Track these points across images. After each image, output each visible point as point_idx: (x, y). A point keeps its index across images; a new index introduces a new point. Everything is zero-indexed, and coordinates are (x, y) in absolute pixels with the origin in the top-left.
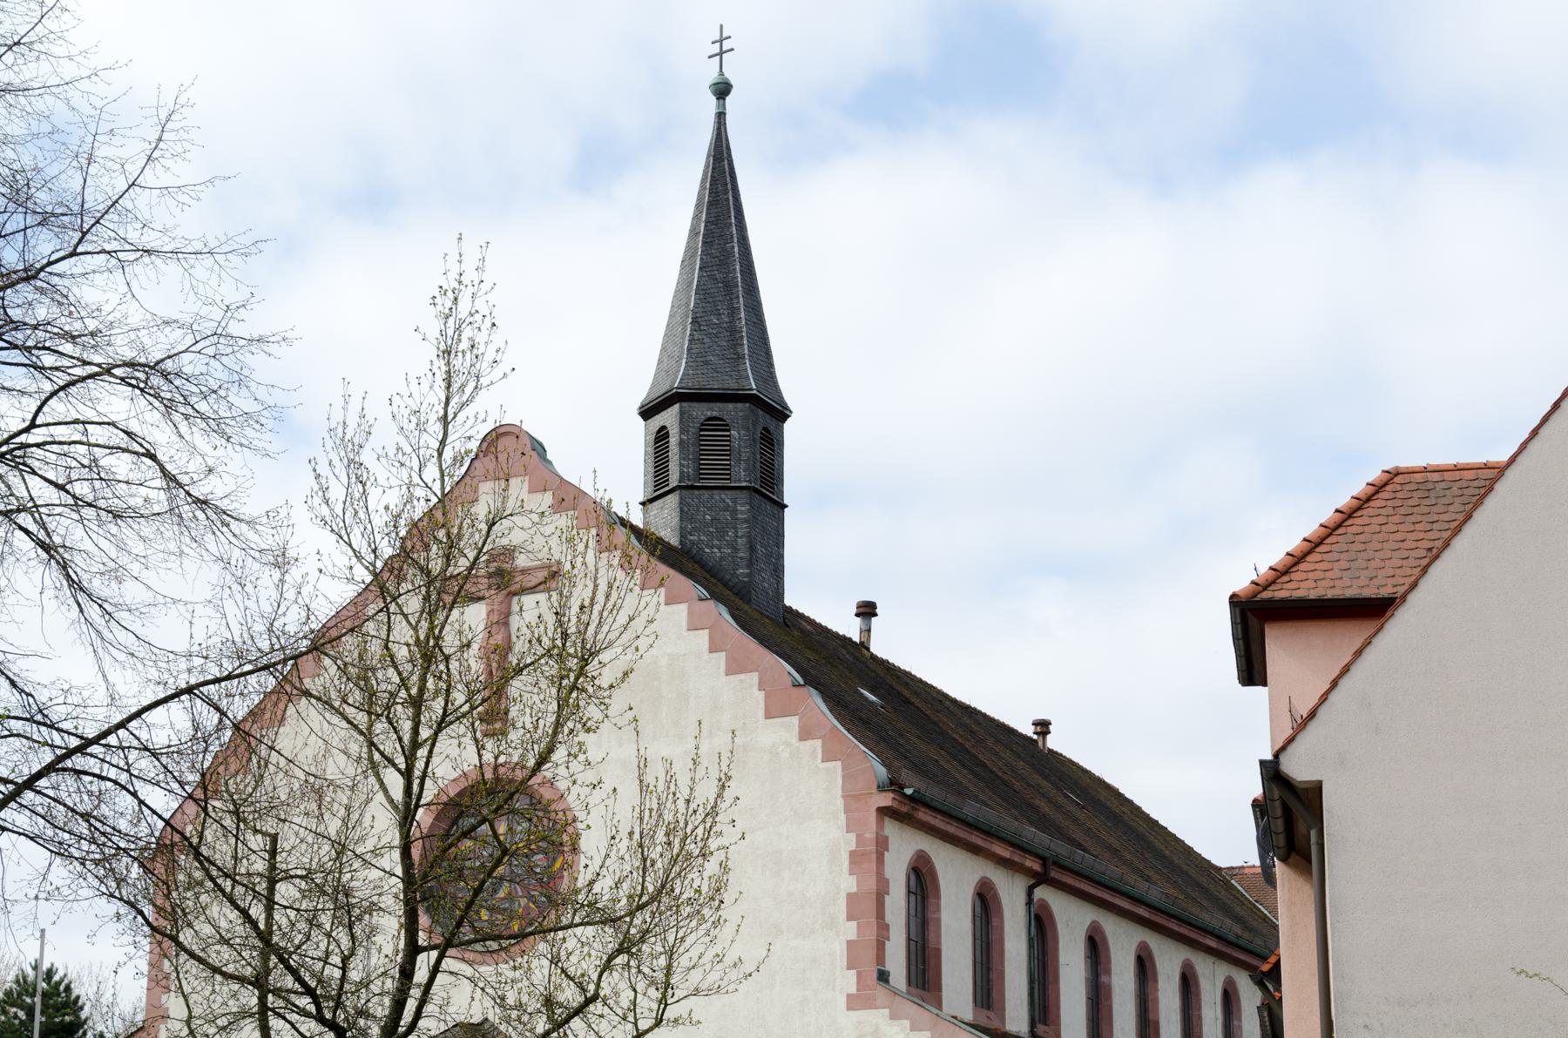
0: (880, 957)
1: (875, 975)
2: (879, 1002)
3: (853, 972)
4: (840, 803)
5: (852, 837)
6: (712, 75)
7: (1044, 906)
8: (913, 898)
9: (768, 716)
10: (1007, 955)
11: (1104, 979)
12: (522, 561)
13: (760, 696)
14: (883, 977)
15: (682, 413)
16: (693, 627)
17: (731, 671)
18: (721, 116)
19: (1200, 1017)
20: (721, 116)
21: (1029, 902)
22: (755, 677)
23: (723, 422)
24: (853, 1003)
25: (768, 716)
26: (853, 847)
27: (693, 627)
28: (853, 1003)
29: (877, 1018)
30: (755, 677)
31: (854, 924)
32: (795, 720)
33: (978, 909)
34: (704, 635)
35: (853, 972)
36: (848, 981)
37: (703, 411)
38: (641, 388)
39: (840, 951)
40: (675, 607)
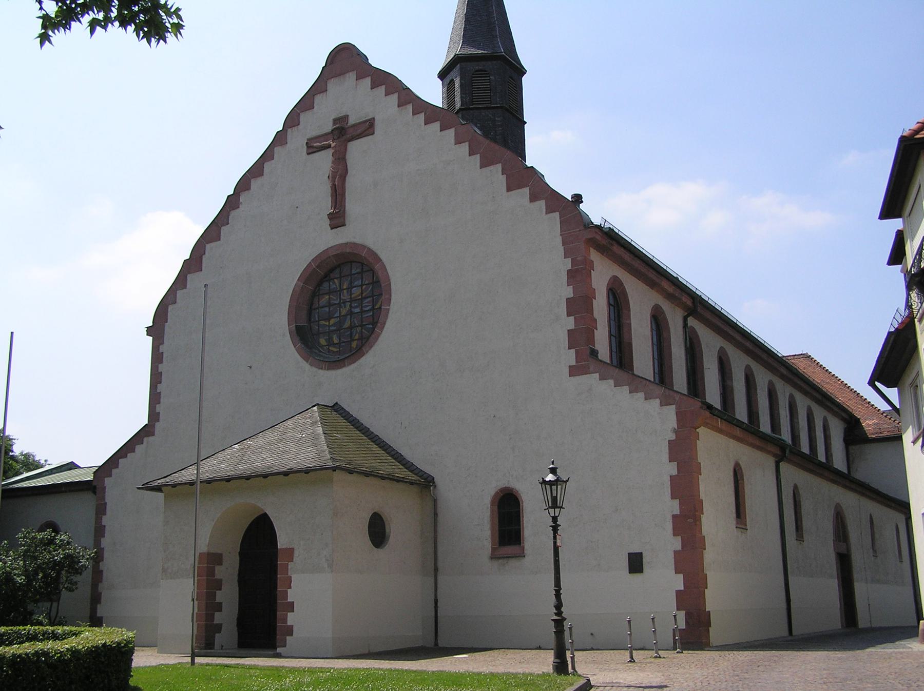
0: (591, 339)
1: (588, 352)
2: (591, 369)
3: (573, 351)
4: (559, 240)
5: (569, 260)
7: (693, 330)
8: (612, 308)
10: (673, 357)
11: (728, 382)
12: (352, 121)
13: (503, 178)
14: (594, 353)
15: (461, 69)
16: (458, 142)
17: (483, 165)
19: (778, 414)
21: (685, 325)
22: (499, 167)
23: (487, 83)
24: (574, 371)
26: (569, 267)
27: (458, 142)
28: (574, 371)
29: (592, 379)
30: (499, 167)
31: (572, 318)
32: (526, 191)
33: (654, 328)
35: (573, 351)
36: (570, 357)
37: (473, 67)
38: (440, 63)
40: (447, 132)
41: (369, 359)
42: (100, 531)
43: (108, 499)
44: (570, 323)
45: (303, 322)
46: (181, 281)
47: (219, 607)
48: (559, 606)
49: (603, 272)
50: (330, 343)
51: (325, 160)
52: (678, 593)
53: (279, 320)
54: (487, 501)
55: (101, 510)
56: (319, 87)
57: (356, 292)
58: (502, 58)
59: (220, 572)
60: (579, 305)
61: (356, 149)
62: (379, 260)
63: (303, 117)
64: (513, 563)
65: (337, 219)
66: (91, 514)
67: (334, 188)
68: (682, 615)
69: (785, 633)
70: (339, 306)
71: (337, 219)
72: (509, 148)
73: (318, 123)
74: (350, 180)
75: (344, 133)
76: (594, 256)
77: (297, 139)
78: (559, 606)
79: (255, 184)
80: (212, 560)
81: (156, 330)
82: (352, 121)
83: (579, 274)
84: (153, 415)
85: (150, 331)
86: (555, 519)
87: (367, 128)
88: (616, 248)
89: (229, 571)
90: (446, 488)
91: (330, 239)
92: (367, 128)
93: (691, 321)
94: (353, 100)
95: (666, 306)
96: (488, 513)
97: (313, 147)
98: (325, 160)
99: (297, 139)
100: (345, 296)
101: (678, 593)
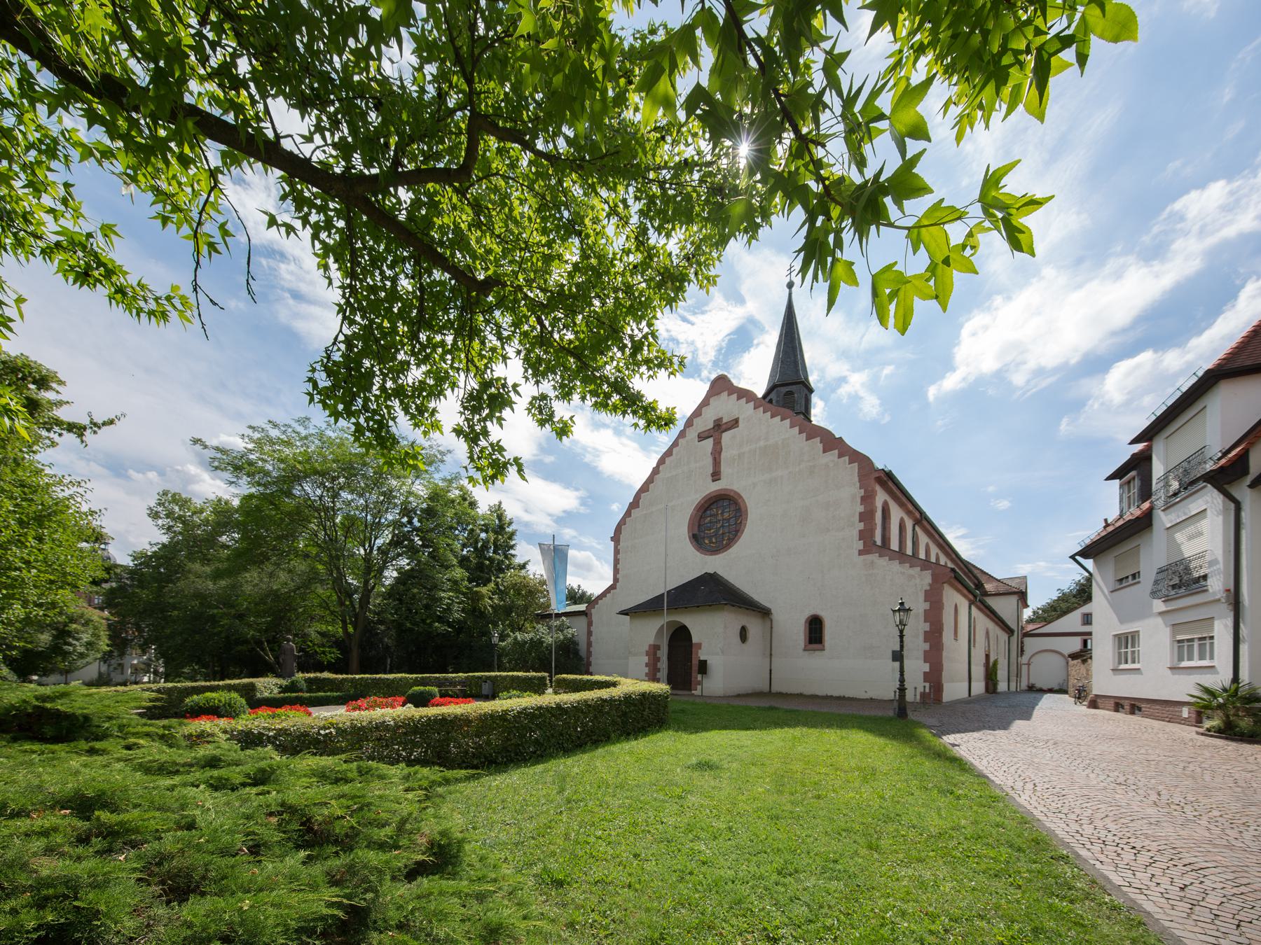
0: (873, 535)
4: (857, 479)
6: (788, 280)
9: (824, 452)
12: (725, 421)
13: (821, 446)
16: (791, 427)
18: (790, 295)
20: (790, 295)
24: (861, 553)
25: (824, 452)
28: (861, 553)
34: (797, 429)
36: (860, 545)
37: (784, 390)
39: (856, 534)
41: (734, 550)
42: (590, 633)
43: (594, 619)
44: (861, 526)
45: (696, 532)
46: (628, 513)
47: (659, 670)
48: (902, 681)
49: (881, 497)
50: (711, 542)
51: (709, 443)
52: (925, 673)
53: (684, 531)
54: (803, 621)
55: (590, 624)
56: (705, 403)
57: (726, 515)
58: (802, 383)
59: (659, 654)
60: (867, 517)
61: (726, 436)
62: (740, 497)
63: (696, 421)
64: (817, 653)
65: (716, 476)
66: (585, 625)
67: (715, 459)
68: (927, 685)
69: (966, 695)
70: (718, 519)
71: (716, 476)
72: (223, 716)
73: (706, 422)
74: (723, 455)
75: (720, 427)
76: (878, 488)
77: (692, 434)
78: (902, 681)
79: (668, 460)
80: (655, 648)
81: (616, 538)
82: (725, 421)
83: (868, 499)
84: (616, 580)
85: (612, 539)
86: (901, 631)
87: (735, 423)
88: (890, 484)
89: (663, 654)
90: (777, 615)
91: (714, 487)
92: (735, 423)
93: (917, 528)
94: (725, 407)
95: (906, 519)
96: (802, 628)
97: (702, 437)
98: (709, 443)
99: (692, 434)
100: (720, 517)
101: (925, 673)
